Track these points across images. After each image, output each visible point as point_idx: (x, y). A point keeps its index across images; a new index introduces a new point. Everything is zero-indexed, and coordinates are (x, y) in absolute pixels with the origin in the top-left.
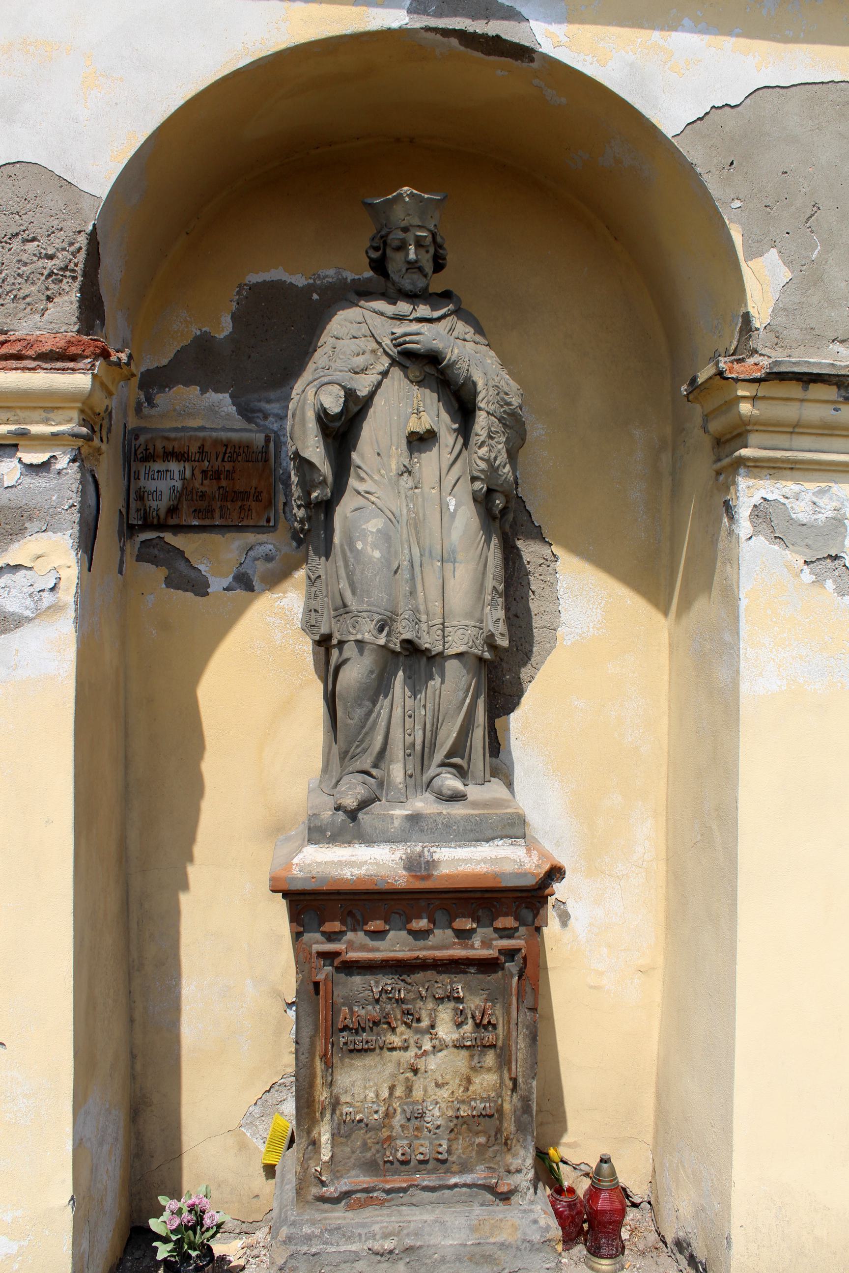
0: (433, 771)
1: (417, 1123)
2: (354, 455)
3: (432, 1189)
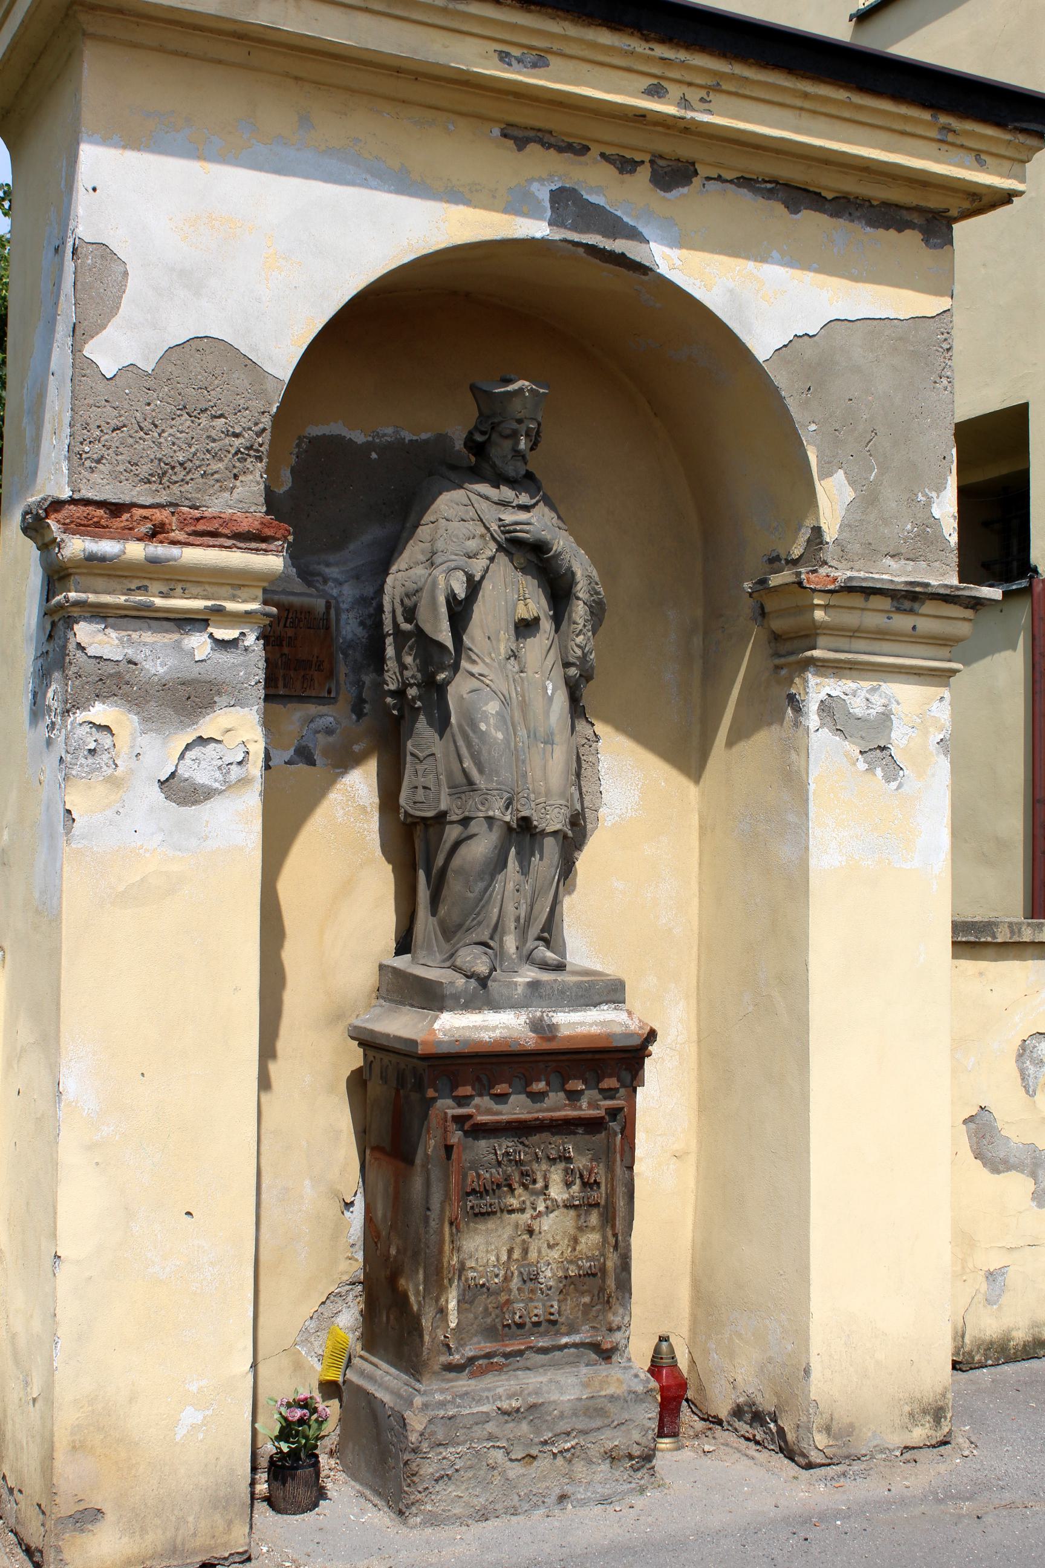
0: (530, 944)
1: (531, 1285)
3: (544, 1351)
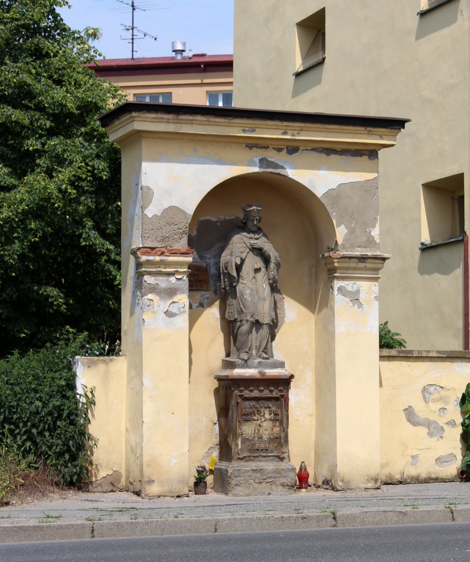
0: (260, 353)
1: (261, 440)
2: (241, 274)
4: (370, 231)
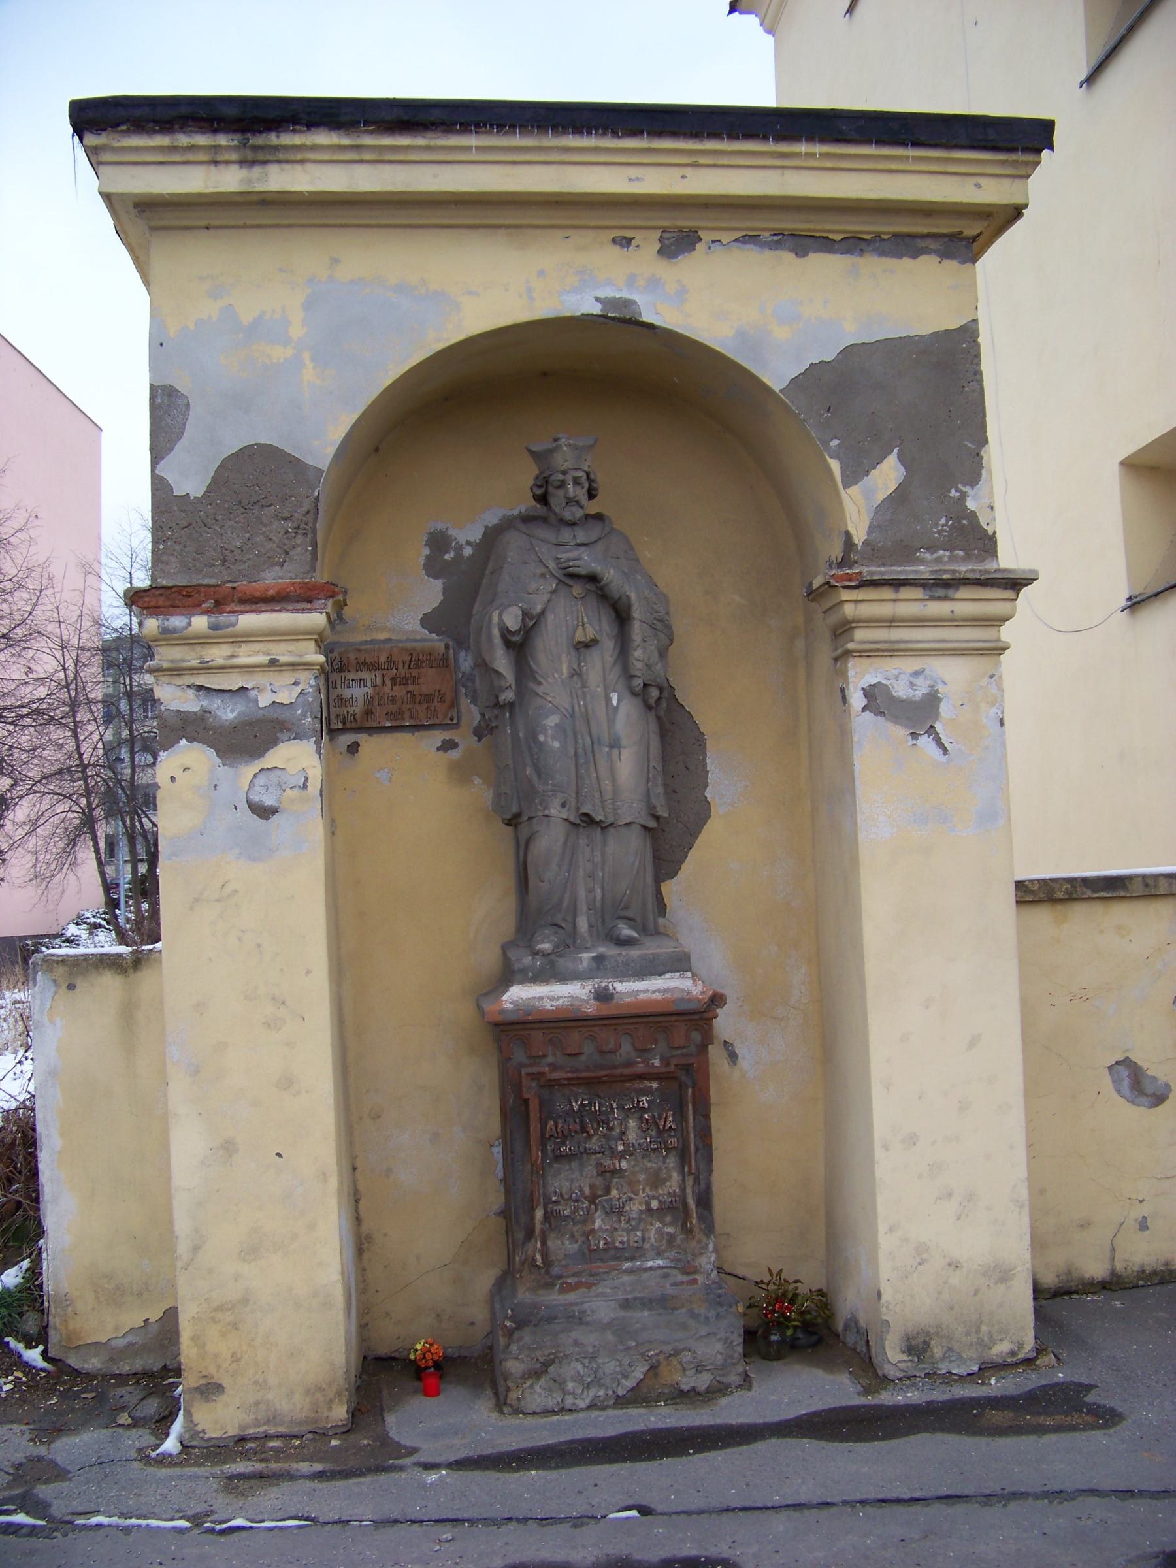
4: (964, 496)
